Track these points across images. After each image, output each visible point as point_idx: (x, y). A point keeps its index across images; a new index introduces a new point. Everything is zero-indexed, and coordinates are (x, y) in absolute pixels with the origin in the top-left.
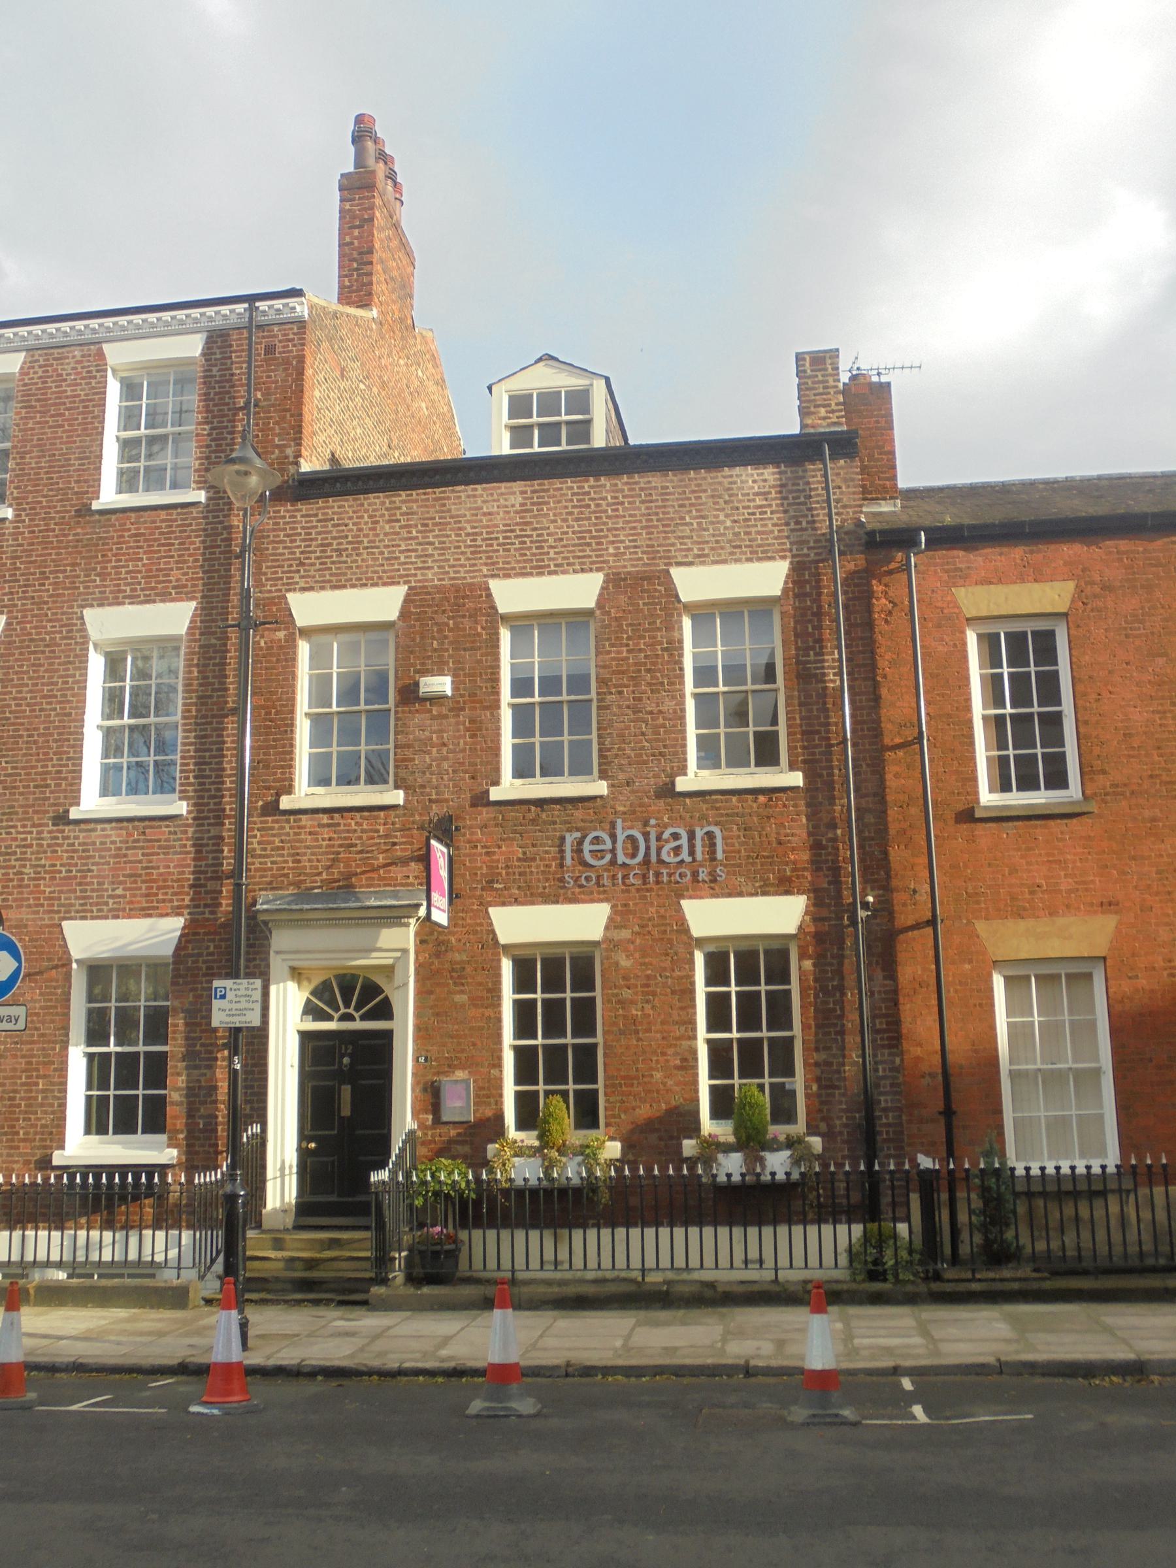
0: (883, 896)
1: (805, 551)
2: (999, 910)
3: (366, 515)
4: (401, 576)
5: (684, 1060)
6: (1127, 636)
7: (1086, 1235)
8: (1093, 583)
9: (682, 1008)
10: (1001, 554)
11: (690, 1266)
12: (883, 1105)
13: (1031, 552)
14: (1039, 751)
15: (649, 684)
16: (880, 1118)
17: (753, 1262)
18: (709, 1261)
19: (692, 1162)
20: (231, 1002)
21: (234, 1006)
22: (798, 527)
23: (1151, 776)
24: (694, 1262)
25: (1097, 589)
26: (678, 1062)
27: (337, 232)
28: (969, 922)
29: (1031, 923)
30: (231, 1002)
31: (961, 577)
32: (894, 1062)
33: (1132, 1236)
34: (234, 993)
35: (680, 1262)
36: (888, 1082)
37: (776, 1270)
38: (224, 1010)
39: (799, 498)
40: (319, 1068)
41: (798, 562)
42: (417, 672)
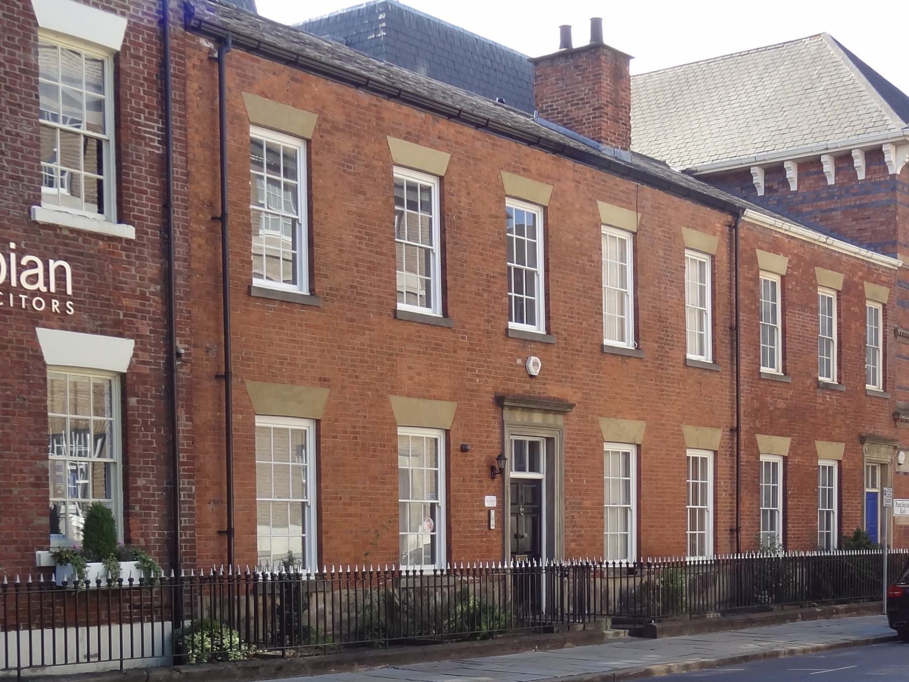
5: (38, 478)
9: (36, 430)
11: (9, 666)
15: (8, 103)
17: (94, 656)
18: (60, 658)
19: (49, 571)
24: (48, 660)
26: (32, 480)
28: (243, 382)
32: (191, 489)
35: (37, 661)
37: (121, 660)
41: (134, 23)
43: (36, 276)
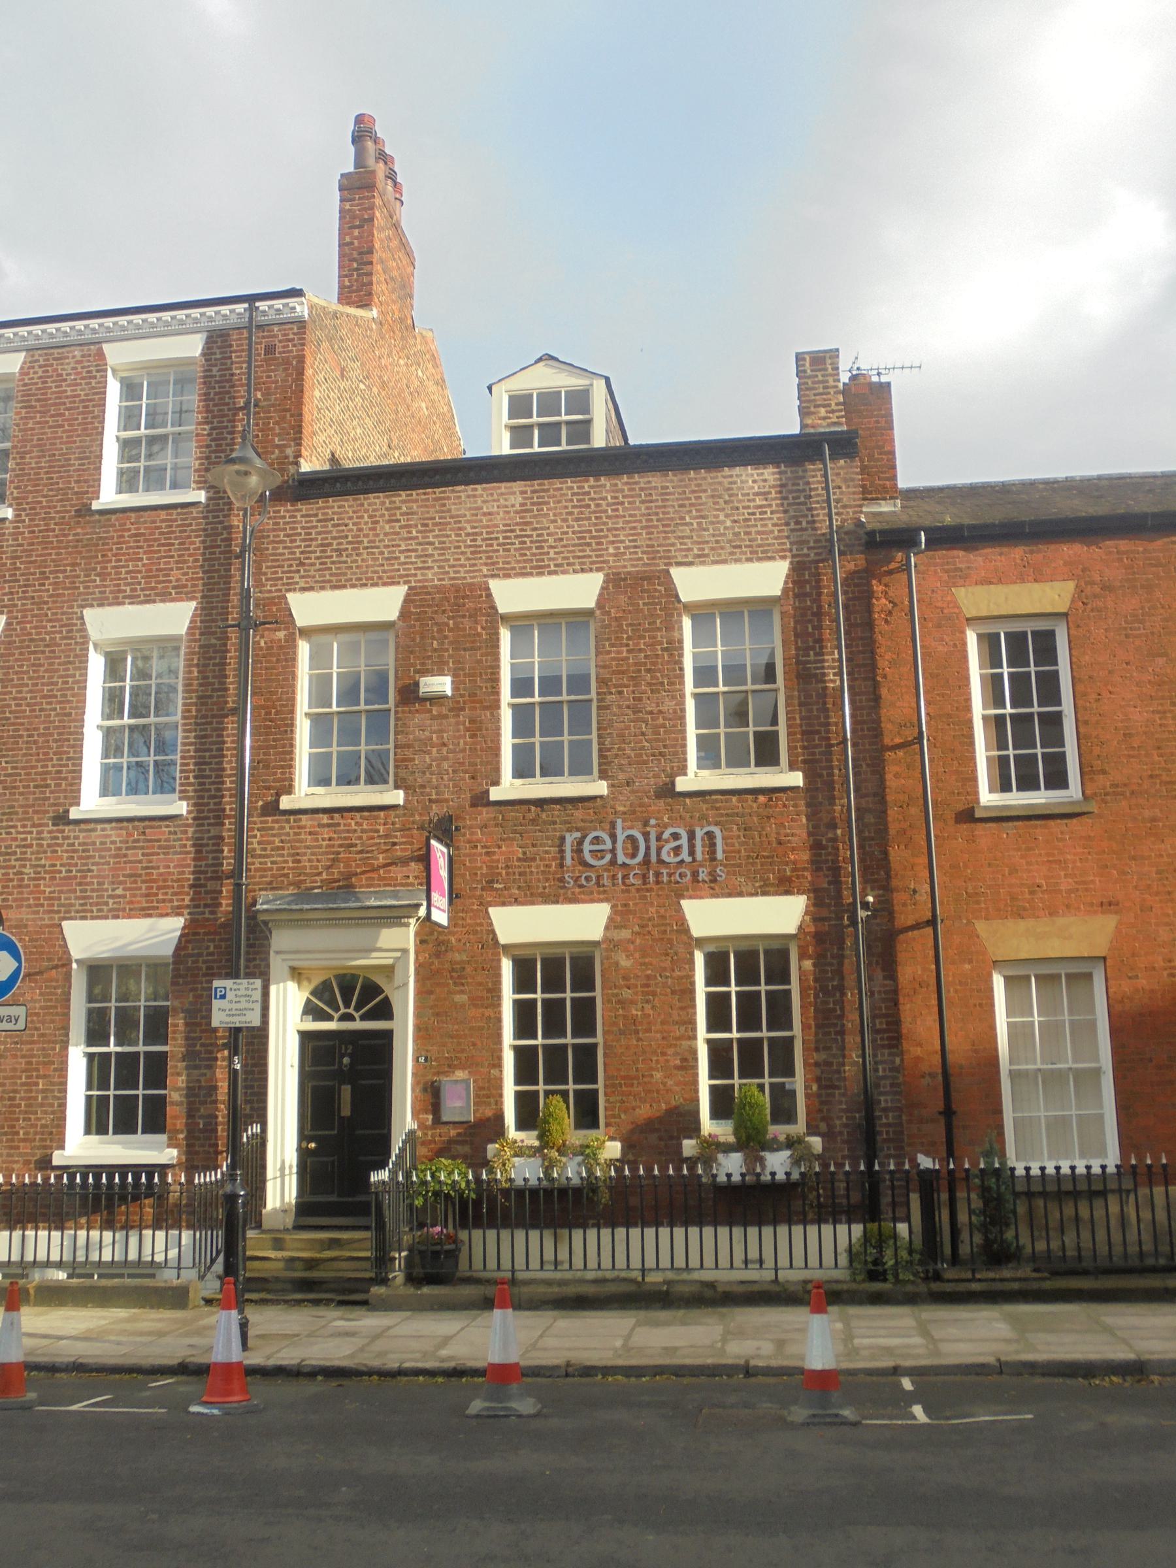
0: (883, 896)
1: (805, 551)
2: (999, 910)
3: (366, 515)
4: (401, 576)
5: (684, 1060)
6: (1127, 636)
7: (1086, 1235)
8: (1093, 583)
9: (682, 1008)
10: (1001, 554)
11: (690, 1266)
12: (883, 1105)
13: (1031, 552)
14: (1039, 751)
15: (649, 684)
16: (880, 1118)
17: (753, 1262)
18: (709, 1261)
19: (692, 1162)
20: (231, 1002)
21: (234, 1006)
22: (798, 527)
23: (1151, 776)
24: (694, 1262)
25: (1097, 589)
26: (678, 1062)
27: (337, 232)
28: (969, 922)
29: (1031, 923)
30: (231, 1002)
31: (961, 577)
32: (894, 1062)
33: (1132, 1236)
34: (234, 993)
35: (680, 1262)
36: (888, 1082)
37: (776, 1270)
38: (224, 1010)
39: (799, 498)
40: (319, 1068)
41: (798, 562)
42: (417, 672)
43: (592, 843)
